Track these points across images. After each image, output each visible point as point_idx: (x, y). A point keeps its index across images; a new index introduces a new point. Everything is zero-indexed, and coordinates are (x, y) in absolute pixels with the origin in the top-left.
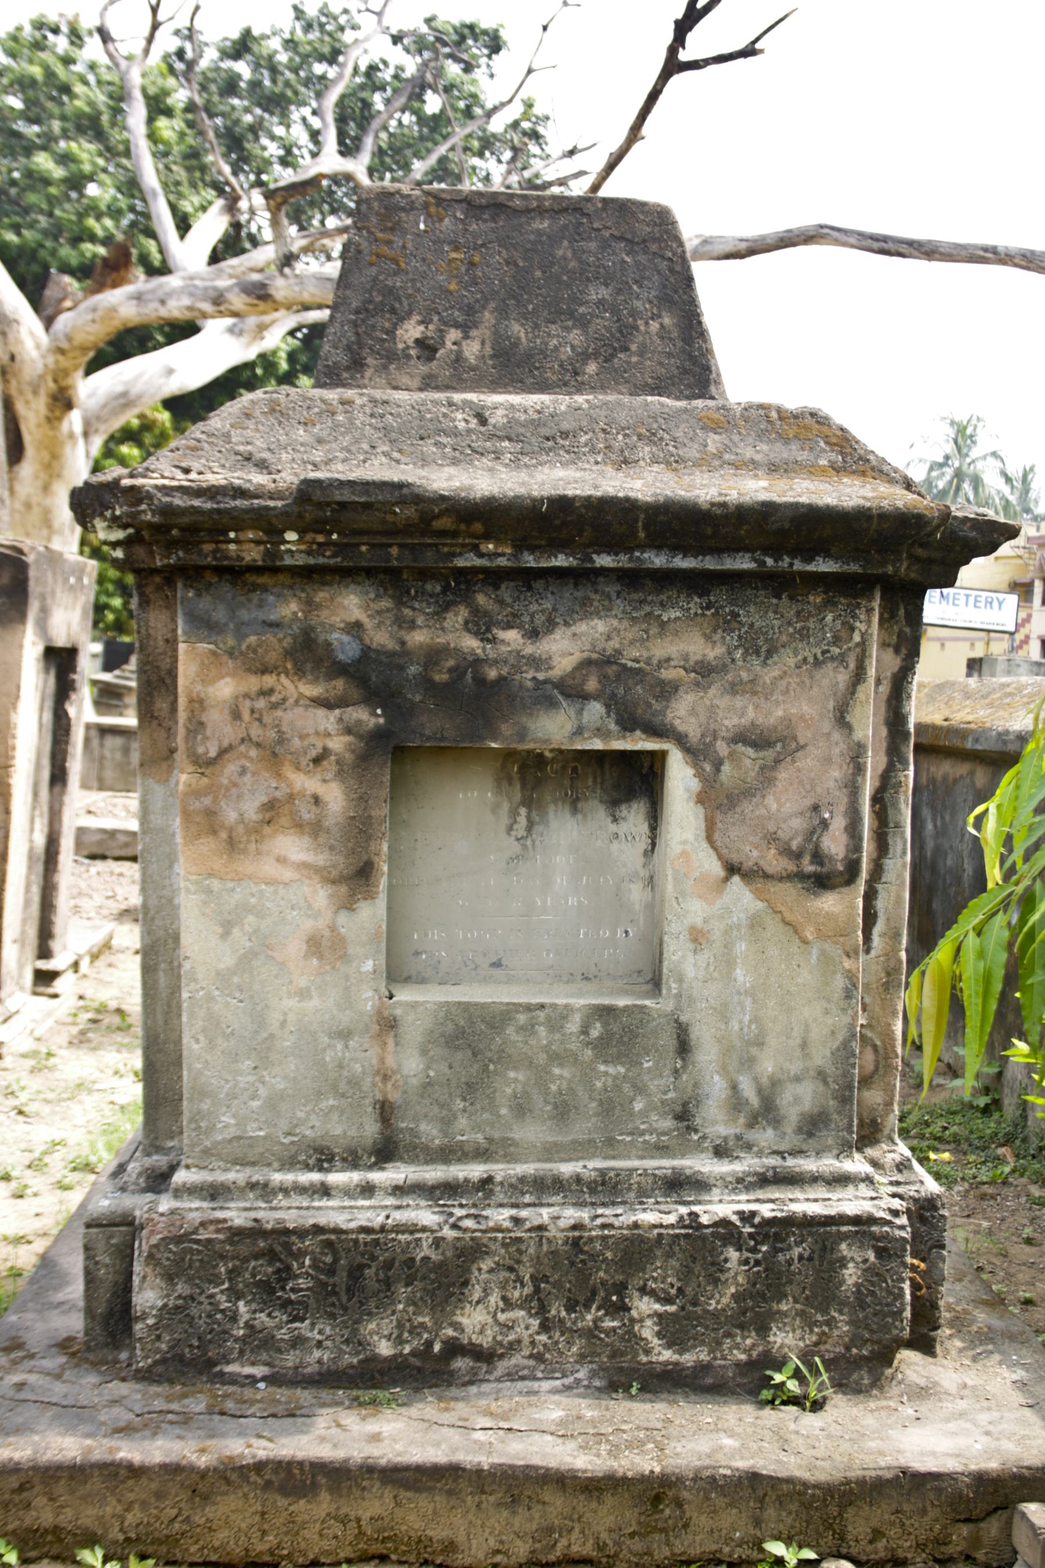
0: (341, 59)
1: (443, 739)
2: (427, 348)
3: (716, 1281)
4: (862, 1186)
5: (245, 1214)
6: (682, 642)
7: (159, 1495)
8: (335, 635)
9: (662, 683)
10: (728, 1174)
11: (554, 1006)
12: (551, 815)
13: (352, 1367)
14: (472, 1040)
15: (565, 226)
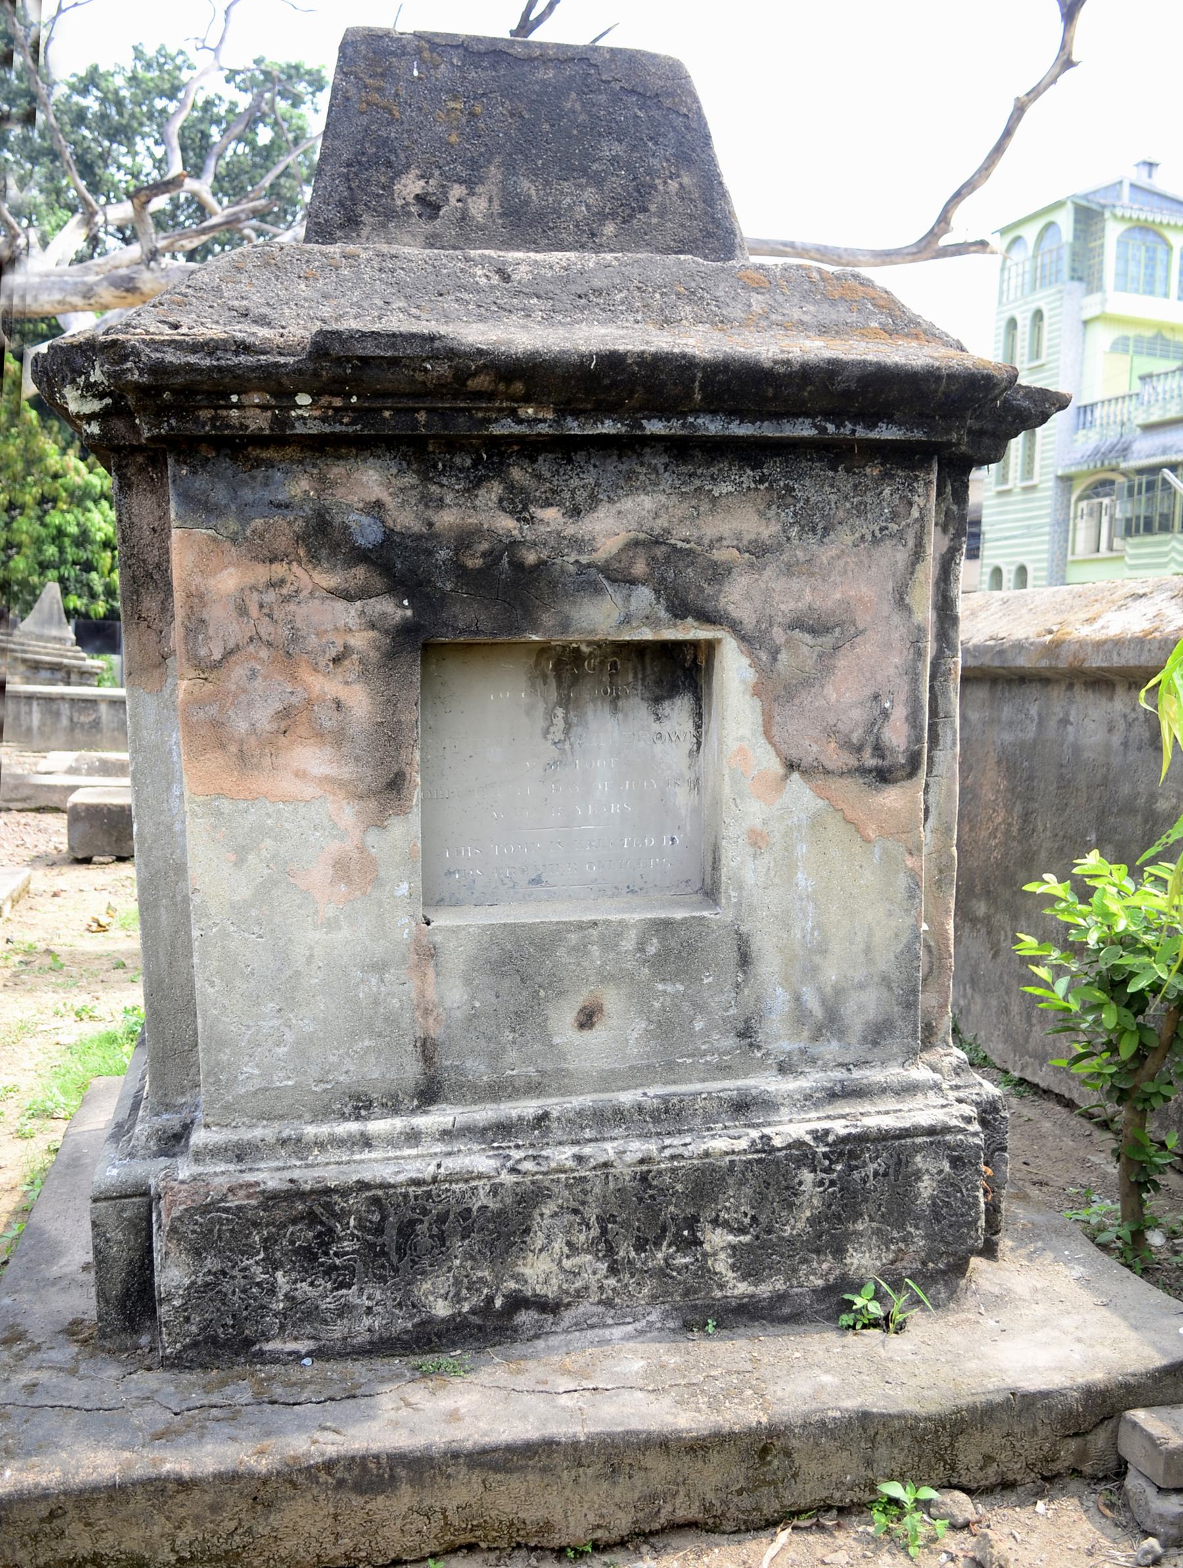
0: (181, 95)
1: (478, 632)
2: (429, 206)
3: (790, 1206)
4: (931, 1093)
5: (278, 1175)
6: (732, 519)
7: (215, 1508)
8: (354, 517)
9: (714, 565)
10: (795, 1091)
11: (607, 923)
12: (590, 713)
13: (407, 1332)
14: (523, 969)
15: (572, 78)
